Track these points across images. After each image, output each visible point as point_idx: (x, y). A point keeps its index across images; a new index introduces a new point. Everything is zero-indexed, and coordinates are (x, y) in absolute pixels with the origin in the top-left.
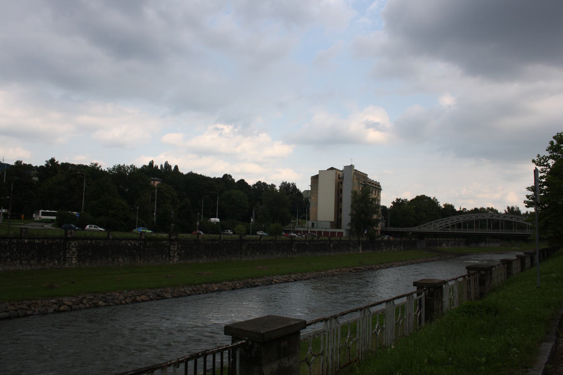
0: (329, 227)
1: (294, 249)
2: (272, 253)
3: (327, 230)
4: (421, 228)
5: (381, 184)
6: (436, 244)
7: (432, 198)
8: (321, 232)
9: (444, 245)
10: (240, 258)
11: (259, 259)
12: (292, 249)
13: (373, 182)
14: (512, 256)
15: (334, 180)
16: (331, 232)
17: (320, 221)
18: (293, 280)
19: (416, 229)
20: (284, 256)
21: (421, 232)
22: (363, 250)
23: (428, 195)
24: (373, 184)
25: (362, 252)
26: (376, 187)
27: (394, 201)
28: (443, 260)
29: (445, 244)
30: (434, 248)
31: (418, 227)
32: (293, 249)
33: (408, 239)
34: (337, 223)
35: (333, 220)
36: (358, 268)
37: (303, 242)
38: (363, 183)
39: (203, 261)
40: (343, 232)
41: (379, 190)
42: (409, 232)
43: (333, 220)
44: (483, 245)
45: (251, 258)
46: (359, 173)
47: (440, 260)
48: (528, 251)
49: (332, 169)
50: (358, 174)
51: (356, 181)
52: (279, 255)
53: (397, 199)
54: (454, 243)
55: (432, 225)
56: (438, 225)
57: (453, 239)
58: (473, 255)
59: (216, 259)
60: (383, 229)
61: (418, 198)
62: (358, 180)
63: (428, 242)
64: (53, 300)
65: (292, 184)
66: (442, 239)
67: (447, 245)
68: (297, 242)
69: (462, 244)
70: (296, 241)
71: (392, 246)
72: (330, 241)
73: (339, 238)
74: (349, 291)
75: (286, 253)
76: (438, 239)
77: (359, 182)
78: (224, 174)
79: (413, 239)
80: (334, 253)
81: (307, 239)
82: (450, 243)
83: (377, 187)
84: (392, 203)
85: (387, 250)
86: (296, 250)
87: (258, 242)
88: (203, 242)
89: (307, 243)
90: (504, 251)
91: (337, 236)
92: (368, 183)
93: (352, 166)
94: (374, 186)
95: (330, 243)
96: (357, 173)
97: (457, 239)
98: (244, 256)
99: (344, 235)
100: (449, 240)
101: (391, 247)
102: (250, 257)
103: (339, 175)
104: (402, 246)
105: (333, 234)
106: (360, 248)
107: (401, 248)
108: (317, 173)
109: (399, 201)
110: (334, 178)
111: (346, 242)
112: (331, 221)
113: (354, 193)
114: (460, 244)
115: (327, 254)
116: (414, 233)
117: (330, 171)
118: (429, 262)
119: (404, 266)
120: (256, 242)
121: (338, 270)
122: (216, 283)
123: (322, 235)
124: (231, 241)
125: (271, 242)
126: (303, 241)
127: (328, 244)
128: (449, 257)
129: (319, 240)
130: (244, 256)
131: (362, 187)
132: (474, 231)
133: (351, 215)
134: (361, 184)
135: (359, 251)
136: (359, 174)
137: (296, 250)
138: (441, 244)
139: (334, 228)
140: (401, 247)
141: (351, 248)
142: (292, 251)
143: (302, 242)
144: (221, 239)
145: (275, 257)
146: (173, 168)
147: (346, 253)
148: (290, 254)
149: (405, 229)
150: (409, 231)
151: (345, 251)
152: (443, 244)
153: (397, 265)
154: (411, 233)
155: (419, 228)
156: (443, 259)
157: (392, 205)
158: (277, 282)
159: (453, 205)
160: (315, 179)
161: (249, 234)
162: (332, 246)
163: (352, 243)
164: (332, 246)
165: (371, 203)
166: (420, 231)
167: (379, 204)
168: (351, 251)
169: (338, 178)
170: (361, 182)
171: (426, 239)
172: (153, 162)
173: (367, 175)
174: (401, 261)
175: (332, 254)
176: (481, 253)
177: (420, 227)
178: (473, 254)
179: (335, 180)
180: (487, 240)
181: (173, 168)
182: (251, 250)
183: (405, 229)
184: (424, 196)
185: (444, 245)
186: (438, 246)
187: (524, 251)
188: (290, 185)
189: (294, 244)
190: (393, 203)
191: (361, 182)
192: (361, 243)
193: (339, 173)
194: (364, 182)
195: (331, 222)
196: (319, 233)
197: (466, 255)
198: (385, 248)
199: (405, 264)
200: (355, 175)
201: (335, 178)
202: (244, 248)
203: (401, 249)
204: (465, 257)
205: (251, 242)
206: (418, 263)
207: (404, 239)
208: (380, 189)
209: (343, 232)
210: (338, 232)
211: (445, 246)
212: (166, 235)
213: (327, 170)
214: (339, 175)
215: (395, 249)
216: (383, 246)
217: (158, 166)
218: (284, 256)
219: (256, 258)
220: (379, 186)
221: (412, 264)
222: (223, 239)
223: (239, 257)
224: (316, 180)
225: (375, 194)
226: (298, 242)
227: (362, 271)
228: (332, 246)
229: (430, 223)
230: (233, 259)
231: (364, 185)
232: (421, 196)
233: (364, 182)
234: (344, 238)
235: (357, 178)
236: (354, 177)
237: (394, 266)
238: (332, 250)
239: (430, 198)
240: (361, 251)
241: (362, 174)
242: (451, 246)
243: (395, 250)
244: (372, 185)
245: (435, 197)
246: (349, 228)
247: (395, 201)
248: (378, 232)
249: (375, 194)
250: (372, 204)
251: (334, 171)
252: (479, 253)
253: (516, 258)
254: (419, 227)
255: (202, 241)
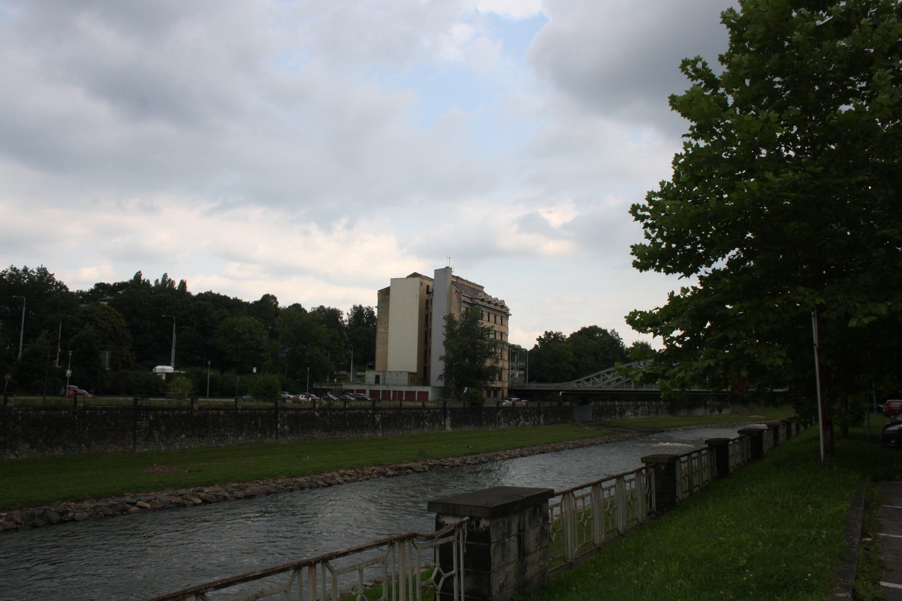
0: (406, 382)
1: (283, 426)
2: (221, 436)
3: (400, 389)
4: (581, 384)
5: (507, 304)
6: (612, 412)
7: (609, 331)
8: (389, 391)
9: (629, 413)
10: (131, 446)
11: (187, 447)
12: (277, 425)
13: (490, 300)
14: (732, 434)
15: (416, 296)
16: (405, 392)
17: (390, 372)
18: (200, 501)
19: (572, 385)
20: (254, 440)
21: (581, 391)
22: (453, 425)
23: (602, 326)
24: (489, 302)
25: (452, 430)
26: (498, 308)
27: (540, 337)
28: (615, 441)
29: (631, 412)
30: (608, 420)
31: (575, 381)
32: (279, 427)
33: (555, 404)
34: (422, 376)
35: (414, 369)
36: (405, 465)
37: (294, 412)
38: (468, 300)
39: (17, 455)
40: (428, 392)
41: (503, 315)
42: (558, 391)
43: (414, 369)
44: (700, 412)
45: (163, 447)
46: (466, 283)
47: (607, 442)
48: (776, 421)
49: (415, 275)
50: (463, 285)
51: (454, 297)
52: (240, 438)
53: (546, 332)
54: (647, 410)
55: (602, 378)
56: (612, 377)
57: (646, 403)
58: (678, 430)
59: (61, 450)
60: (515, 386)
61: (584, 331)
62: (459, 295)
63: (597, 408)
64: (4, 513)
65: (367, 309)
66: (624, 403)
67: (635, 414)
68: (290, 412)
69: (662, 410)
70: (285, 409)
71: (521, 418)
72: (375, 410)
73: (420, 404)
74: (102, 572)
75: (259, 435)
76: (617, 404)
77: (460, 298)
78: (264, 294)
79: (567, 404)
80: (385, 433)
81: (317, 406)
82: (640, 409)
83: (501, 311)
84: (538, 340)
85: (509, 424)
86: (286, 427)
87: (184, 412)
88: (20, 412)
89: (317, 414)
90: (734, 423)
91: (393, 398)
92: (477, 301)
93: (448, 270)
94: (491, 306)
95: (374, 414)
96: (459, 283)
97: (654, 403)
98: (142, 442)
99: (430, 397)
100: (639, 404)
101: (517, 420)
102: (161, 444)
103: (428, 286)
104: (541, 418)
105: (410, 395)
106: (448, 422)
107: (540, 421)
108: (388, 284)
109: (550, 337)
110: (417, 293)
111: (414, 411)
112: (410, 371)
113: (450, 319)
114: (660, 410)
115: (367, 435)
116: (569, 394)
117: (411, 279)
118: (582, 446)
119: (524, 459)
120: (178, 412)
121: (350, 472)
122: (303, 475)
123: (390, 399)
124: (106, 409)
125: (222, 412)
126: (306, 409)
127: (369, 416)
128: (627, 435)
129: (347, 406)
130: (142, 442)
131: (467, 308)
132: (623, 388)
133: (446, 359)
134: (464, 302)
135: (445, 428)
136: (466, 286)
137: (286, 427)
138: (622, 413)
139: (417, 385)
140: (539, 418)
141: (426, 423)
142: (277, 429)
143: (303, 412)
144: (78, 405)
145: (231, 443)
146: (177, 285)
147: (413, 431)
148: (270, 436)
149: (553, 386)
150: (558, 389)
151: (411, 428)
152: (627, 412)
153: (506, 457)
154: (562, 394)
155: (578, 384)
156: (614, 440)
157: (537, 343)
158: (145, 508)
159: (649, 344)
160: (384, 295)
161: (203, 394)
162: (378, 418)
163: (427, 413)
164: (378, 419)
165: (482, 337)
166: (581, 389)
167: (503, 339)
168: (425, 428)
169: (426, 292)
170: (463, 298)
171: (593, 403)
172: (141, 274)
173: (483, 287)
174: (521, 447)
175: (380, 434)
176: (693, 427)
177: (579, 382)
178: (678, 429)
179: (418, 296)
180: (708, 403)
181: (177, 285)
182: (164, 428)
183: (553, 386)
184: (596, 327)
185: (630, 414)
186: (617, 416)
187: (768, 422)
188: (364, 310)
189: (282, 416)
190: (540, 339)
191: (463, 298)
192: (449, 412)
193: (426, 282)
194: (471, 299)
195: (410, 373)
196: (386, 393)
197: (663, 431)
198: (505, 422)
199: (525, 452)
200: (453, 286)
201: (418, 292)
202: (144, 424)
203: (539, 422)
204: (662, 435)
205: (165, 412)
206: (558, 451)
207: (548, 404)
208: (505, 313)
209: (428, 392)
210: (418, 392)
211: (631, 415)
212: (131, 398)
213: (408, 277)
214: (428, 286)
215: (527, 423)
216: (499, 418)
217: (150, 281)
218: (254, 440)
219: (178, 447)
220: (503, 306)
221: (543, 453)
222: (82, 405)
223: (129, 444)
224: (387, 296)
225: (489, 321)
226: (294, 412)
227: (414, 471)
228: (378, 418)
229: (597, 374)
230: (109, 451)
231: (472, 305)
232: (591, 327)
233: (471, 299)
234: (431, 402)
235: (456, 291)
236: (451, 289)
237: (498, 458)
238: (380, 427)
239: (605, 332)
240: (448, 428)
241: (471, 286)
242: (641, 415)
243: (526, 425)
244: (487, 305)
245: (614, 330)
246: (441, 384)
247: (543, 337)
248: (503, 390)
249: (489, 321)
250: (484, 339)
251: (417, 279)
252: (689, 427)
253: (738, 436)
254: (577, 382)
255: (17, 410)
